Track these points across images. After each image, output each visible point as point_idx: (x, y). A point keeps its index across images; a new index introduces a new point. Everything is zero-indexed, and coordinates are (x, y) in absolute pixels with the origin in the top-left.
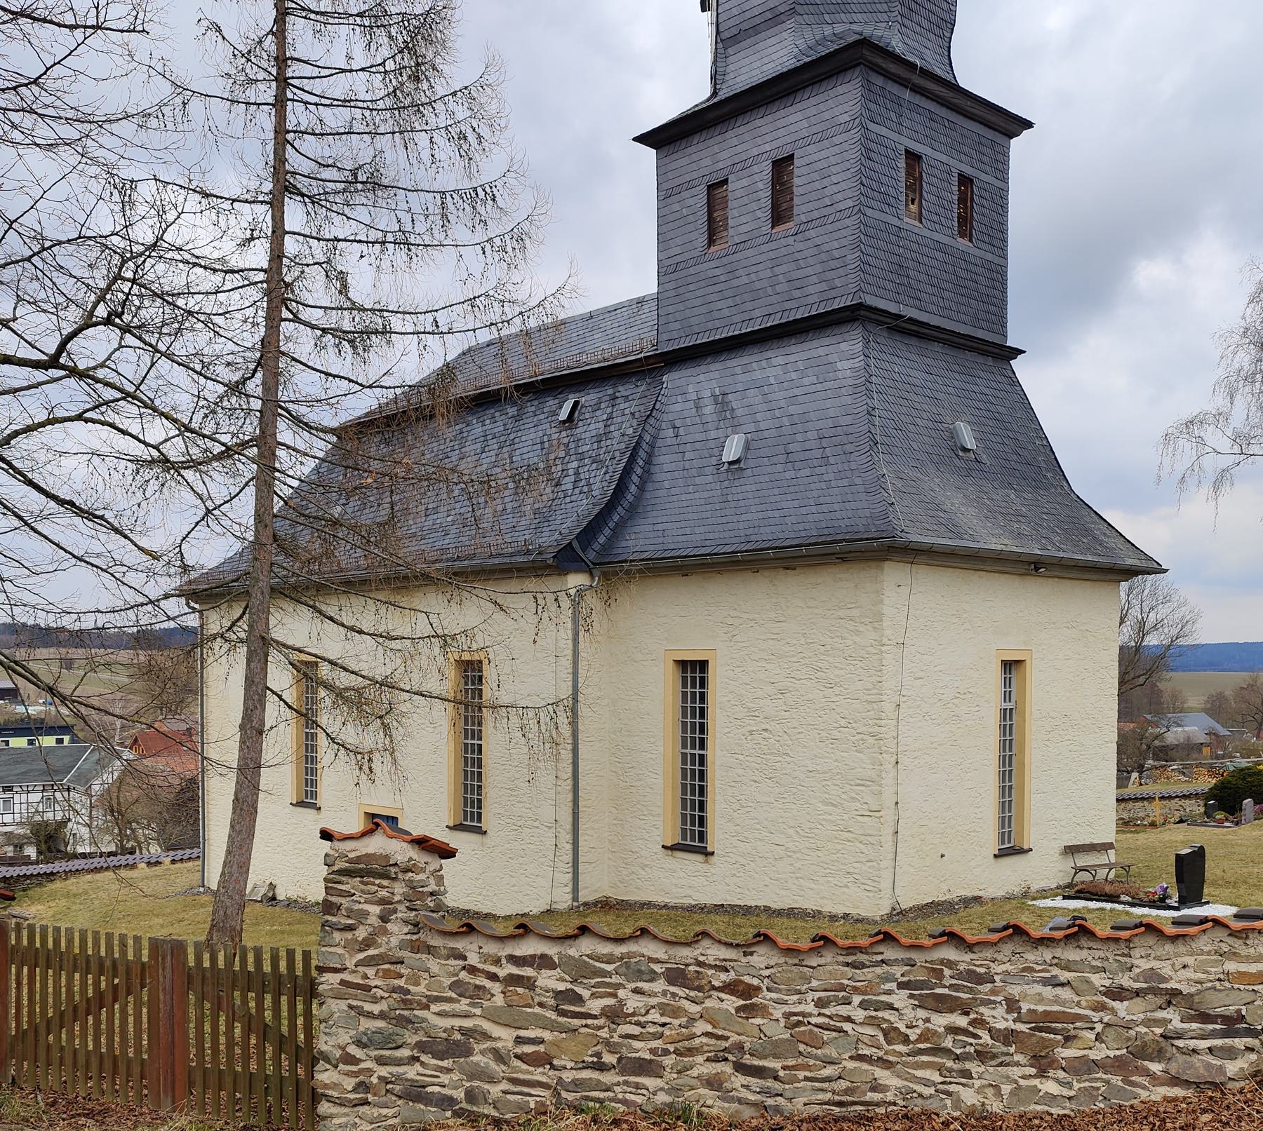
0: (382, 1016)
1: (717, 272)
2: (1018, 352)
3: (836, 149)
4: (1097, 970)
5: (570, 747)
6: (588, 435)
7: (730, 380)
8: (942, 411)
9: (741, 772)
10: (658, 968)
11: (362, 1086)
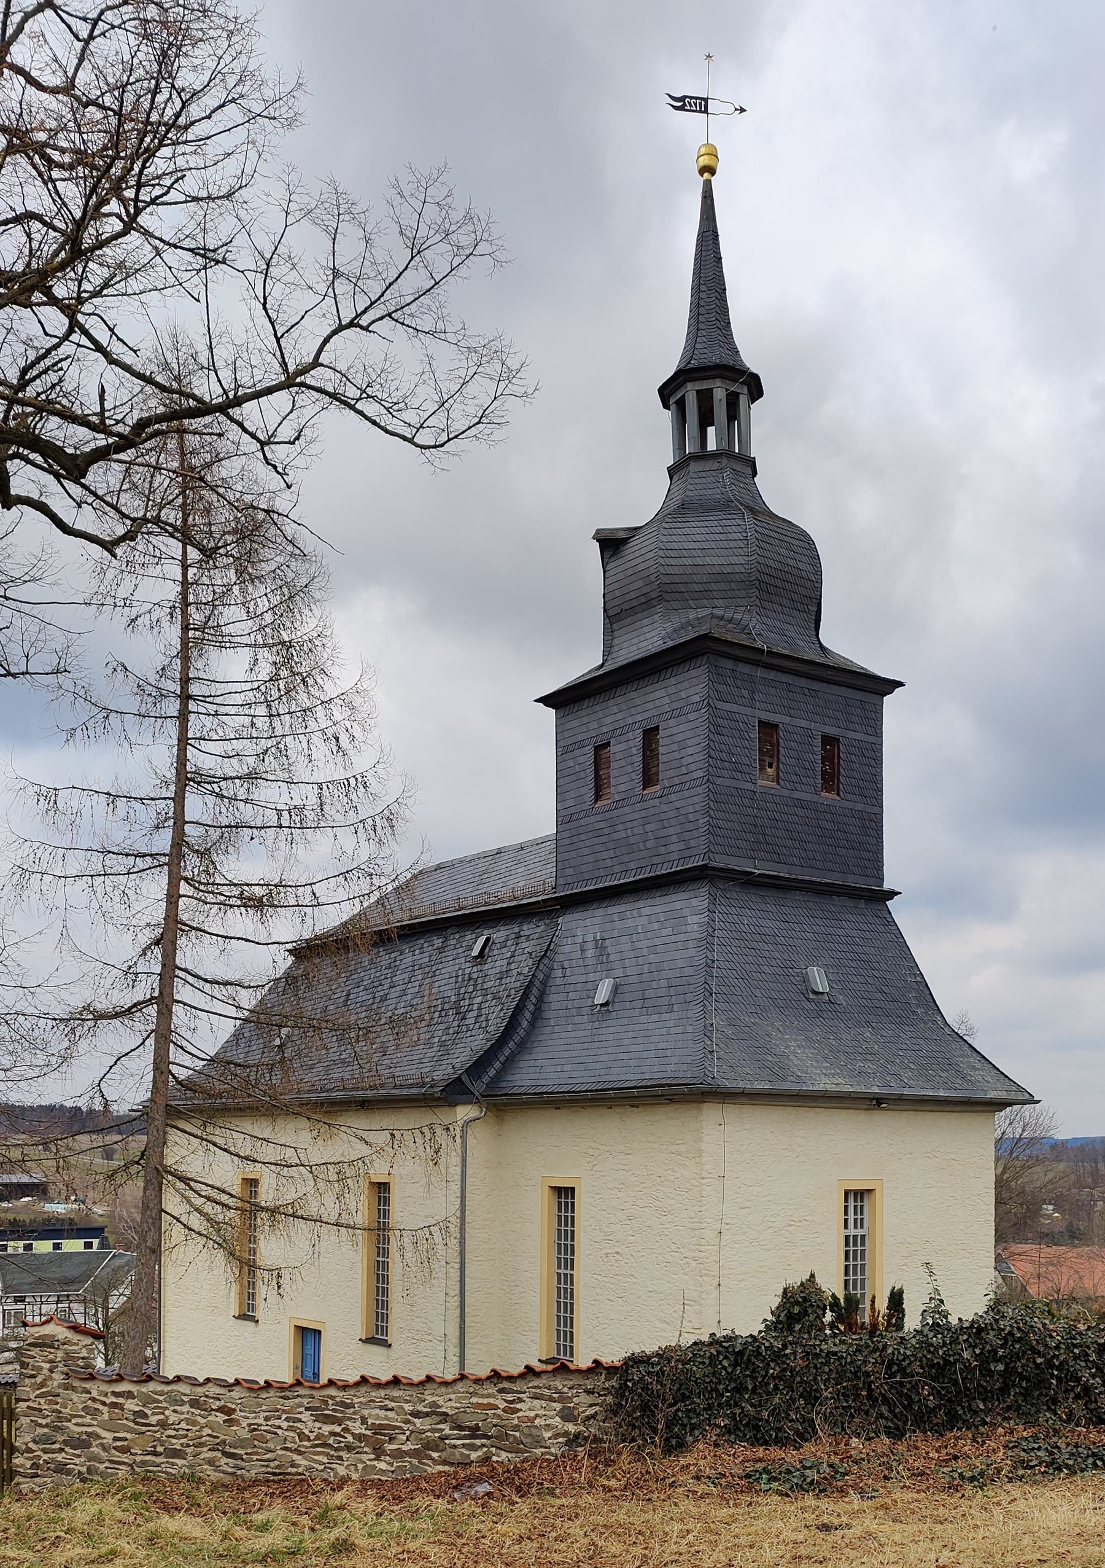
0: (47, 1426)
1: (602, 825)
2: (892, 894)
3: (690, 725)
4: (407, 1402)
5: (457, 1266)
6: (492, 971)
7: (608, 926)
8: (795, 957)
9: (599, 1291)
10: (185, 1399)
11: (35, 1466)
